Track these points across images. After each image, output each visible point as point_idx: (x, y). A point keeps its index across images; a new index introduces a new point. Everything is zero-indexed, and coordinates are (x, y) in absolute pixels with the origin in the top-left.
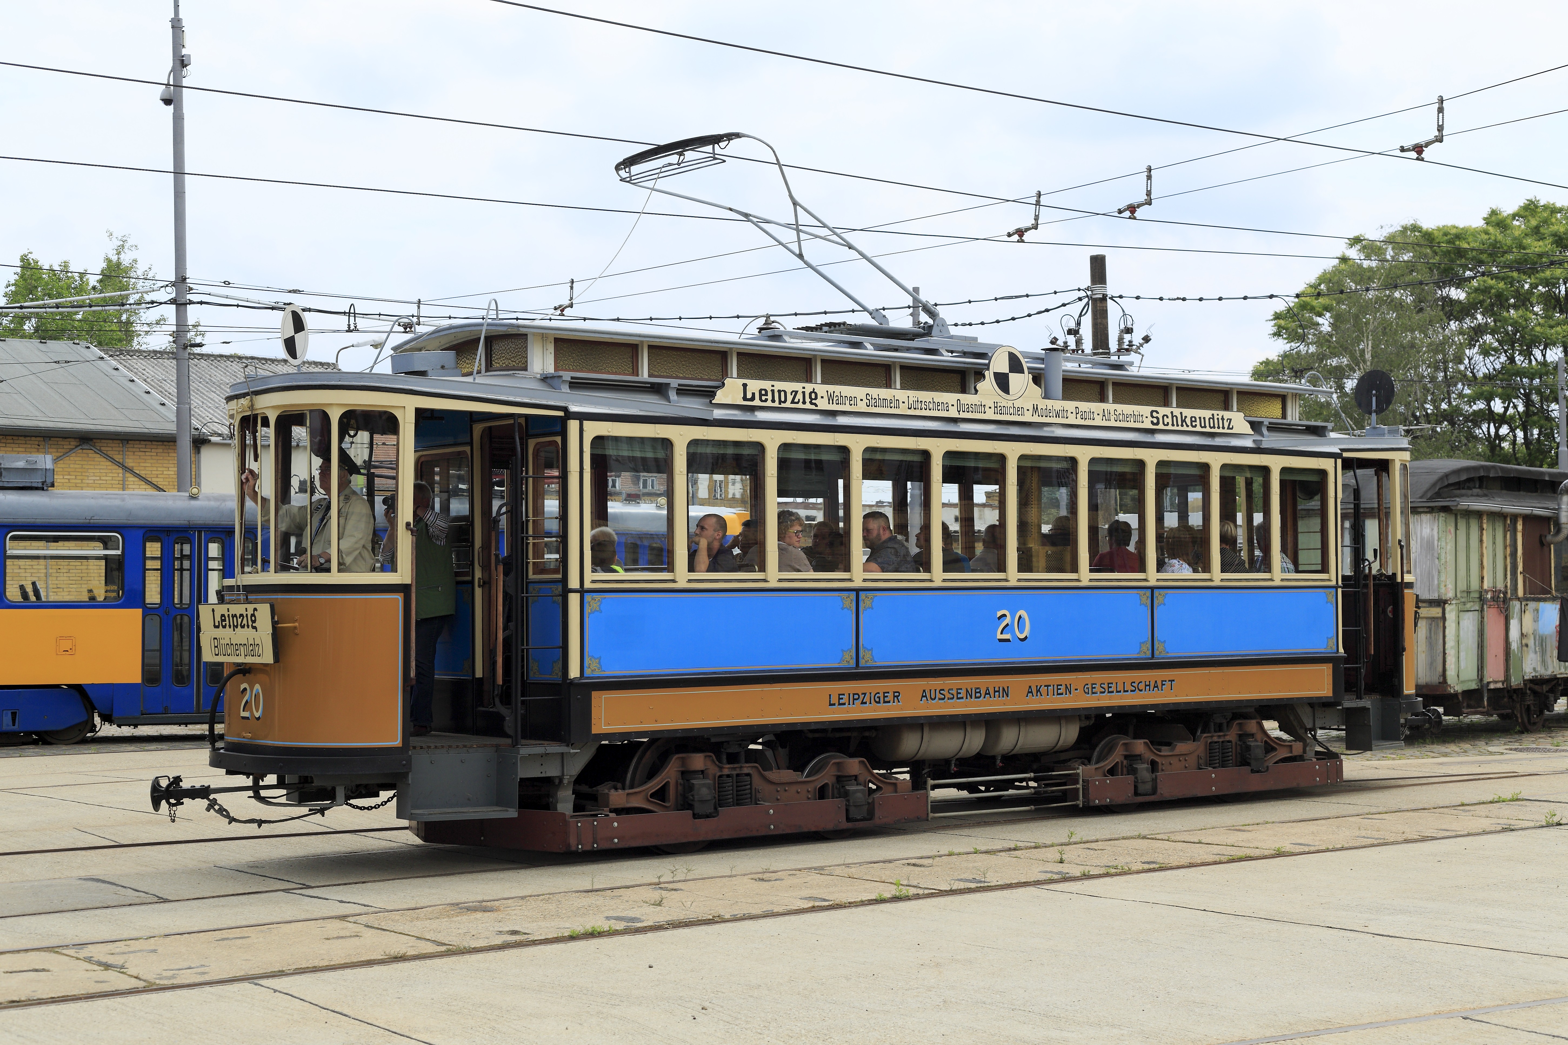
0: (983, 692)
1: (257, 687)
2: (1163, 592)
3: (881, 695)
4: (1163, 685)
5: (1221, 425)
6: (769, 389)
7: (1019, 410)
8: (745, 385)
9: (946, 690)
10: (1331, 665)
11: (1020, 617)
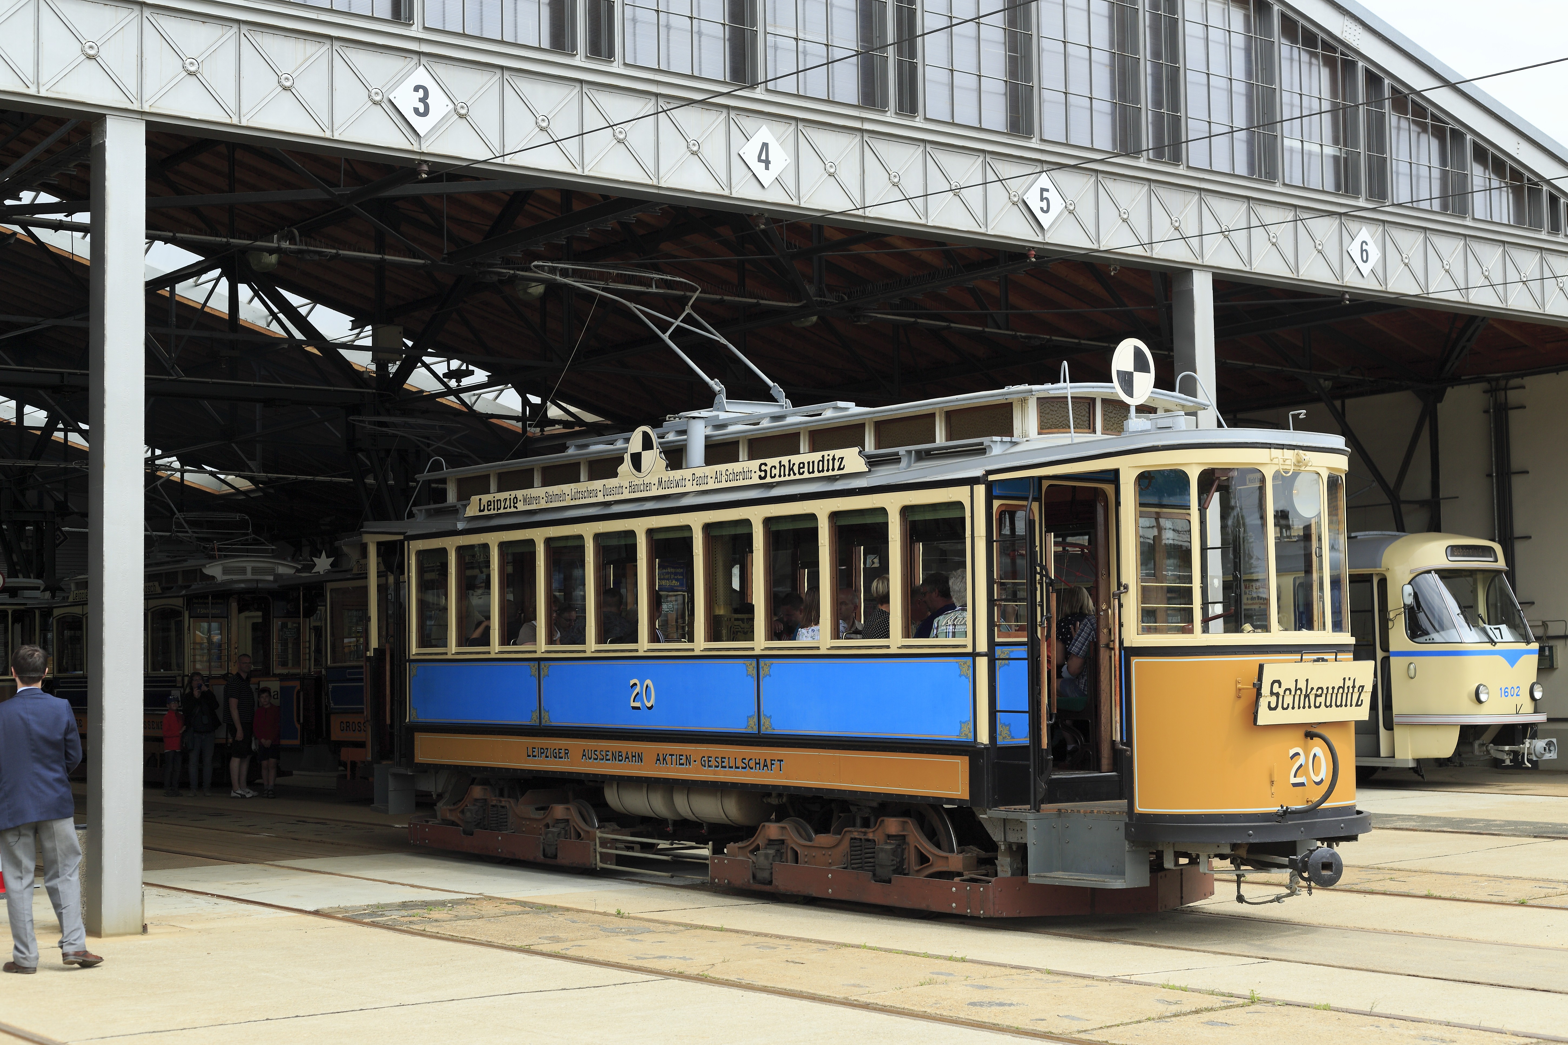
1: (648, 682)
2: (547, 663)
3: (557, 751)
4: (772, 764)
5: (831, 467)
7: (647, 486)
8: (480, 500)
10: (967, 758)
11: (1315, 755)
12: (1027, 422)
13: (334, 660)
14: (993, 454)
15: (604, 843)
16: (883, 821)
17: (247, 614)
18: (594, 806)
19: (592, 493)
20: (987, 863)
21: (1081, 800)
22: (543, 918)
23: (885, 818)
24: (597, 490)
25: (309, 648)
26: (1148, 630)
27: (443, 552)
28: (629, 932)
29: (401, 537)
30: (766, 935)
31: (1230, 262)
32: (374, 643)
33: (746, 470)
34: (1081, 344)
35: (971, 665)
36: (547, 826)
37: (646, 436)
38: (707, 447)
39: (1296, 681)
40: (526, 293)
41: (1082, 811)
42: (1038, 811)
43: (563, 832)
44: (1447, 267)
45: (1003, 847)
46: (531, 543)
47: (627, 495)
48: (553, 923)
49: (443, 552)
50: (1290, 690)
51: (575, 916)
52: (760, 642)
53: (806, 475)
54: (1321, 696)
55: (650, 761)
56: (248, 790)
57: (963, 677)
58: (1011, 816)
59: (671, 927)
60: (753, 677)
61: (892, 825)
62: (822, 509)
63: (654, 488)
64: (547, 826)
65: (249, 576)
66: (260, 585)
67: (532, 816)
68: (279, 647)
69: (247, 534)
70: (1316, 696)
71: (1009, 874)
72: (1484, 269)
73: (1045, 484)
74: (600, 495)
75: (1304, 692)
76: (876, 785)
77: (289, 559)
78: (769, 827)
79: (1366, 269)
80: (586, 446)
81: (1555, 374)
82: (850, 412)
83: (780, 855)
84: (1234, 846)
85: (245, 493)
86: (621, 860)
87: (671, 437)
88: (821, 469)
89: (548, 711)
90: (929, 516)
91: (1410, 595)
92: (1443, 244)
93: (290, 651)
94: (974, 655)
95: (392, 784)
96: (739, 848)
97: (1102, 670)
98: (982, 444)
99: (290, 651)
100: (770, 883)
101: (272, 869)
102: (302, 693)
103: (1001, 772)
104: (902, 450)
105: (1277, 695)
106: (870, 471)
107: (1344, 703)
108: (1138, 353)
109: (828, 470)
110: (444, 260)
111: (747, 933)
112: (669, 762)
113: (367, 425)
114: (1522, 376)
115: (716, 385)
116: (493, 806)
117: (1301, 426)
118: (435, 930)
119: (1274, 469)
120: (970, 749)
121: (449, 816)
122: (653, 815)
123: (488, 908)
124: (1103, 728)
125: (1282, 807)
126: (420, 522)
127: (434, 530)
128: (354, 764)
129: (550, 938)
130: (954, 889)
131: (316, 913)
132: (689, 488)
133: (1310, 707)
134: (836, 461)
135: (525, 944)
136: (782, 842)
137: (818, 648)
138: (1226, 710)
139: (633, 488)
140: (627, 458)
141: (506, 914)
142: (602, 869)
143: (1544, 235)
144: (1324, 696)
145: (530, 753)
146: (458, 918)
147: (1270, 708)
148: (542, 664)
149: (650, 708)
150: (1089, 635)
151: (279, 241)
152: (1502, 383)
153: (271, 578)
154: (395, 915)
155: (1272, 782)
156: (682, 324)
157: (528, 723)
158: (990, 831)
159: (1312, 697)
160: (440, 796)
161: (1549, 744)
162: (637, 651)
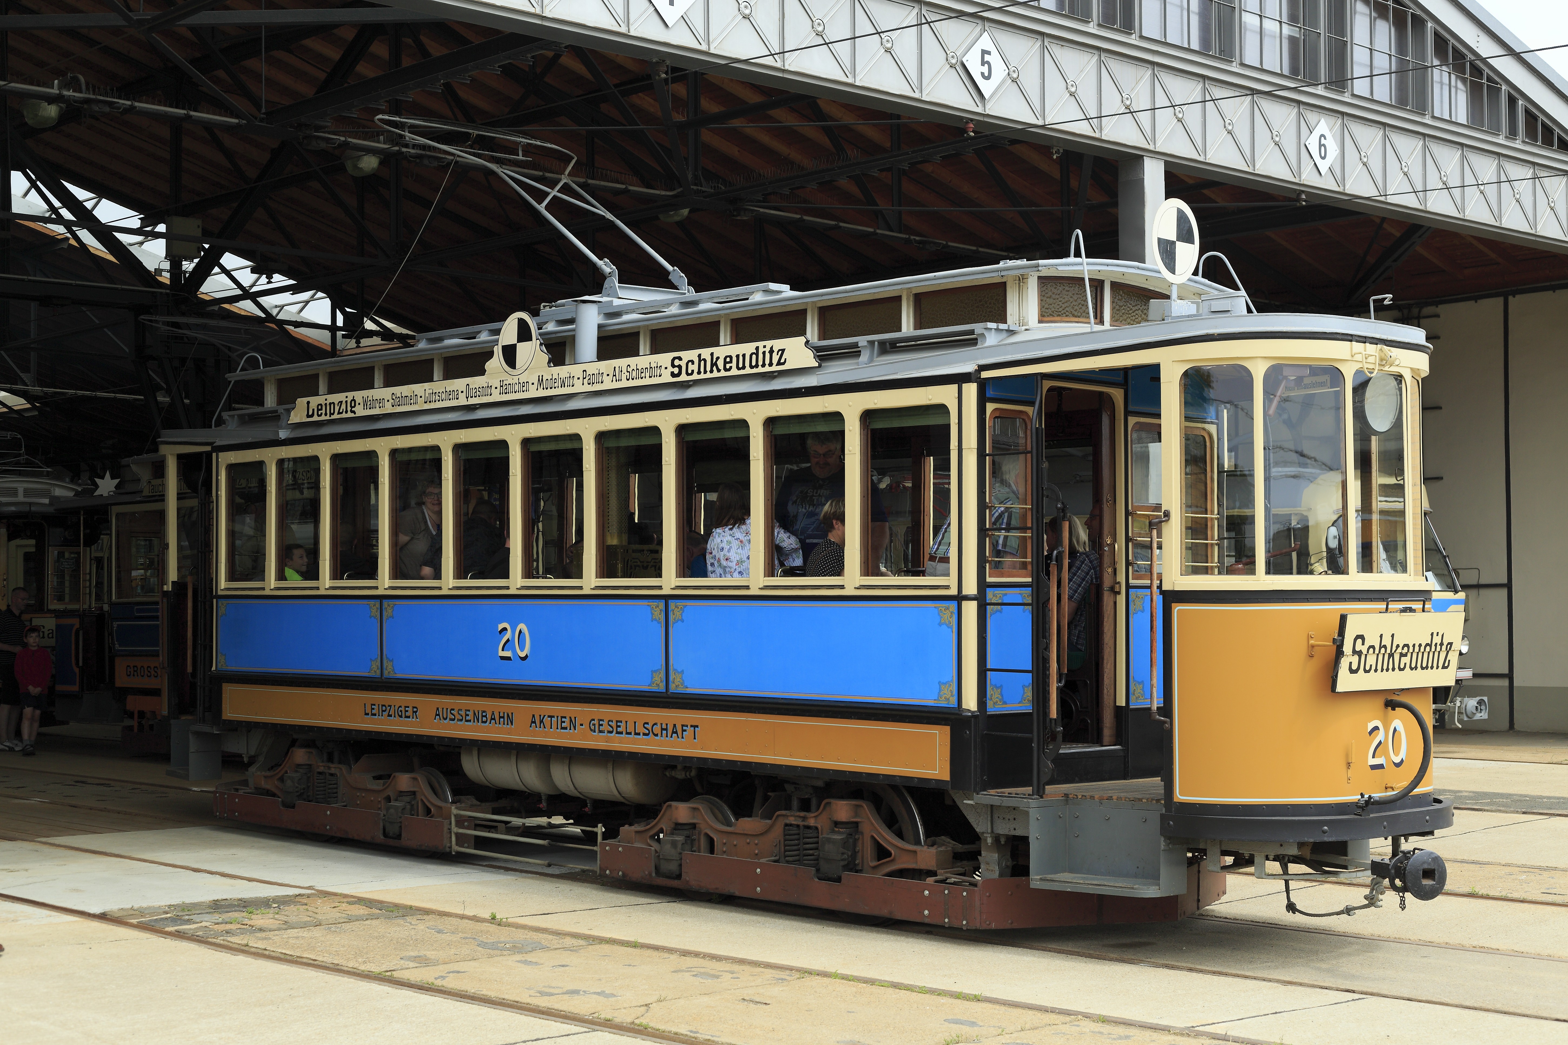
0: (489, 716)
2: (681, 603)
3: (402, 709)
4: (683, 731)
5: (767, 362)
6: (344, 400)
7: (524, 385)
8: (308, 403)
9: (456, 710)
11: (520, 632)
12: (1025, 307)
13: (119, 594)
14: (987, 344)
15: (461, 821)
16: (829, 803)
17: (18, 542)
18: (445, 774)
19: (455, 394)
20: (968, 859)
21: (1081, 781)
22: (399, 925)
23: (833, 801)
24: (460, 390)
25: (90, 580)
26: (1196, 571)
27: (259, 465)
28: (516, 948)
29: (209, 448)
30: (697, 954)
31: (1183, 149)
32: (173, 575)
33: (653, 366)
34: (979, 252)
35: (956, 611)
36: (388, 799)
37: (522, 323)
38: (600, 339)
39: (1381, 636)
40: (356, 167)
41: (1096, 797)
42: (1042, 797)
43: (408, 807)
44: (1406, 170)
45: (989, 840)
46: (372, 455)
47: (496, 397)
48: (413, 933)
49: (259, 465)
50: (1373, 647)
51: (440, 923)
52: (670, 579)
53: (734, 372)
54: (1406, 655)
55: (522, 725)
56: (16, 742)
57: (944, 627)
58: (996, 801)
59: (569, 941)
60: (659, 623)
61: (842, 810)
62: (754, 415)
63: (533, 388)
64: (388, 799)
65: (21, 498)
66: (33, 509)
67: (369, 787)
68: (55, 579)
69: (20, 455)
70: (1402, 655)
71: (996, 875)
72: (1443, 174)
73: (1047, 384)
74: (462, 397)
75: (1388, 651)
76: (822, 759)
77: (67, 480)
78: (677, 808)
79: (1324, 166)
80: (441, 339)
81: (1473, 302)
82: (783, 295)
83: (690, 841)
84: (1301, 845)
85: (19, 412)
86: (480, 843)
87: (551, 327)
88: (754, 363)
89: (392, 661)
90: (896, 423)
91: (1335, 537)
92: (1403, 142)
93: (67, 584)
94: (960, 598)
95: (193, 745)
96: (637, 832)
97: (1105, 620)
98: (972, 332)
99: (67, 584)
100: (679, 877)
101: (46, 849)
102: (81, 633)
103: (992, 746)
104: (862, 340)
105: (1359, 653)
106: (820, 366)
107: (1430, 665)
108: (1181, 217)
109: (763, 365)
110: (261, 120)
111: (670, 950)
112: (548, 724)
113: (160, 325)
114: (1437, 304)
115: (606, 266)
116: (320, 773)
117: (1383, 313)
118: (261, 945)
119: (1356, 367)
120: (953, 717)
121: (264, 784)
122: (523, 788)
123: (325, 910)
124: (1105, 691)
125: (1362, 795)
126: (231, 430)
127: (250, 440)
128: (142, 714)
129: (415, 959)
130: (927, 892)
131: (103, 917)
132: (579, 388)
133: (1393, 669)
134: (774, 354)
135: (384, 968)
136: (694, 826)
137: (747, 587)
138: (1295, 673)
139: (504, 388)
140: (498, 351)
141: (350, 920)
142: (458, 853)
143: (1501, 140)
144: (1409, 655)
145: (368, 711)
146: (288, 926)
147: (1352, 671)
148: (386, 603)
149: (524, 659)
150: (1087, 574)
151: (60, 88)
152: (1415, 311)
153: (46, 501)
154: (207, 921)
155: (1349, 765)
156: (559, 195)
157: (366, 674)
158: (972, 819)
159: (1397, 657)
160: (252, 761)
161: (1480, 702)
162: (508, 588)
